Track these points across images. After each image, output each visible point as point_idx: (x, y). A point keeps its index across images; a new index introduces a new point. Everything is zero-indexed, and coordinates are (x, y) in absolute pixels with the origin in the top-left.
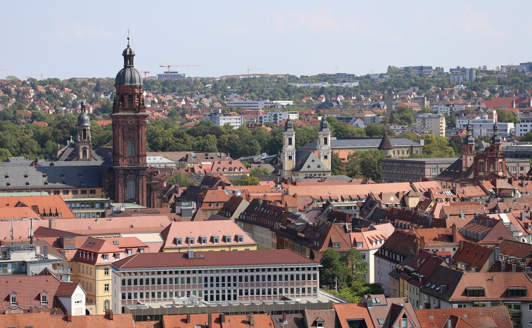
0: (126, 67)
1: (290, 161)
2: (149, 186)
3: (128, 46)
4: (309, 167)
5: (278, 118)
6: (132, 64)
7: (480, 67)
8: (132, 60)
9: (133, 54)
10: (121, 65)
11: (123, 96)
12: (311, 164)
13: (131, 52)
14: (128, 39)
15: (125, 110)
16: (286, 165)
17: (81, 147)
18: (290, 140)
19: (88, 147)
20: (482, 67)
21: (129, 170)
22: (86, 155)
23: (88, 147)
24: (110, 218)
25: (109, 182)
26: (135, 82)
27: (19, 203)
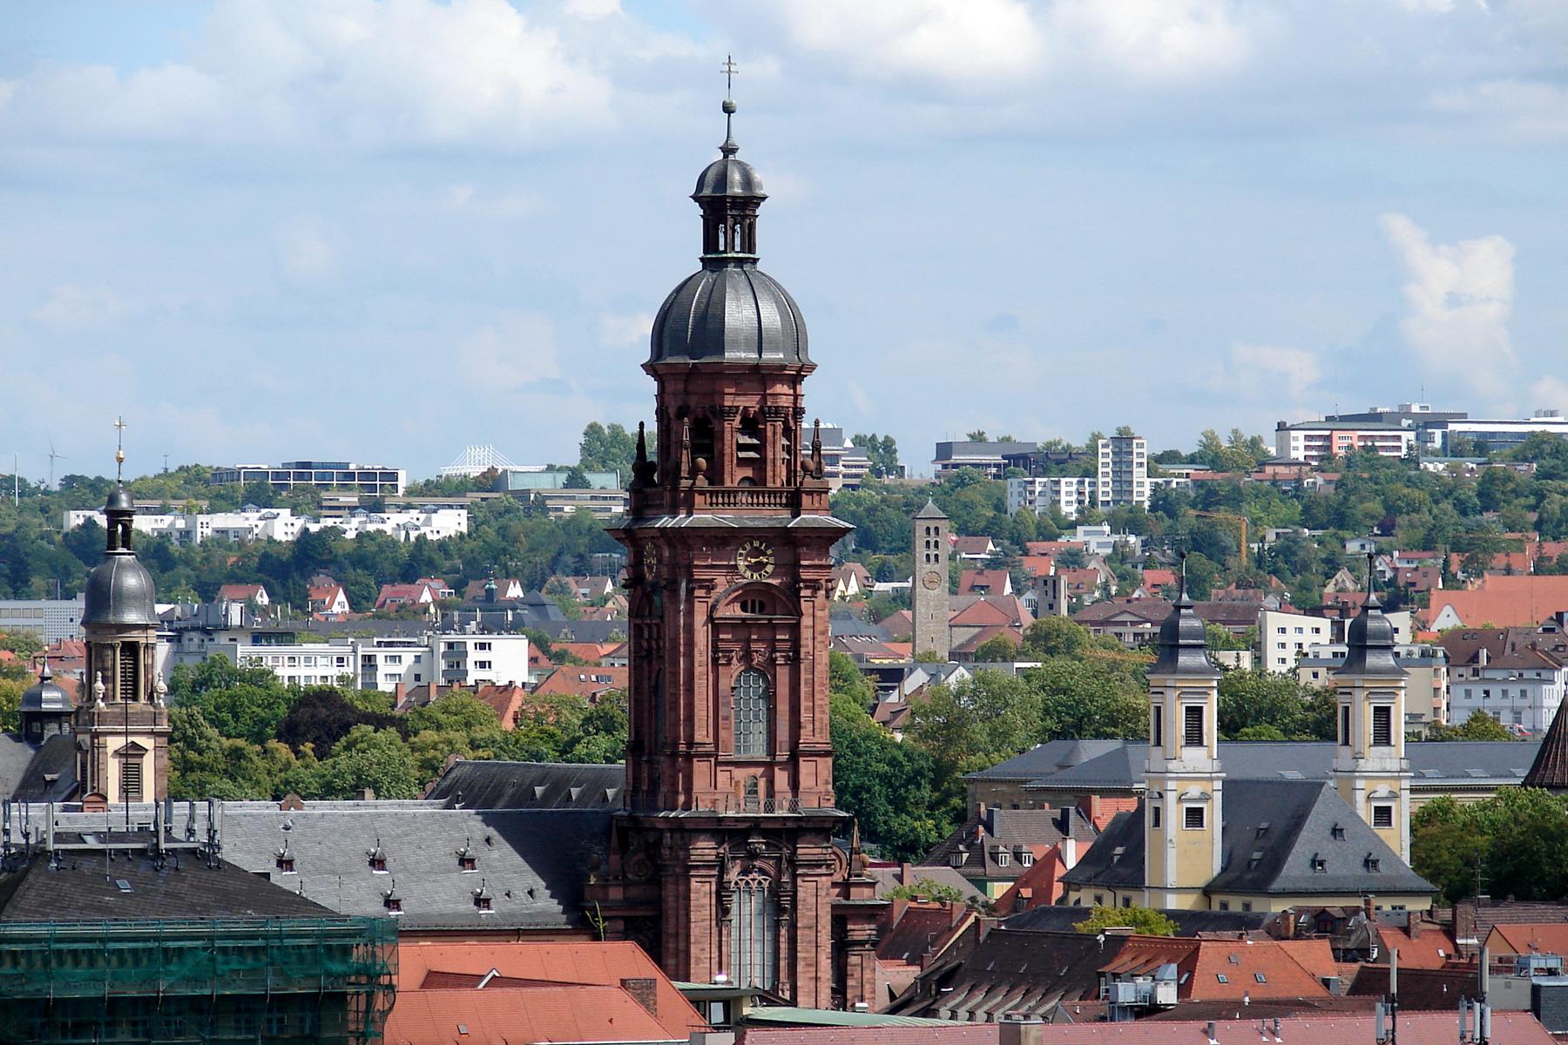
0: (713, 261)
1: (1195, 833)
2: (841, 917)
3: (728, 150)
4: (1316, 863)
5: (470, 665)
6: (751, 249)
7: (874, 437)
8: (752, 227)
9: (759, 192)
10: (682, 253)
11: (707, 421)
12: (1328, 849)
13: (748, 182)
14: (728, 109)
15: (722, 495)
16: (1172, 854)
17: (114, 743)
18: (1195, 713)
19: (147, 742)
20: (881, 439)
21: (746, 833)
22: (139, 790)
23: (147, 742)
24: (1269, 1022)
25: (628, 902)
26: (720, 348)
27: (431, 974)
